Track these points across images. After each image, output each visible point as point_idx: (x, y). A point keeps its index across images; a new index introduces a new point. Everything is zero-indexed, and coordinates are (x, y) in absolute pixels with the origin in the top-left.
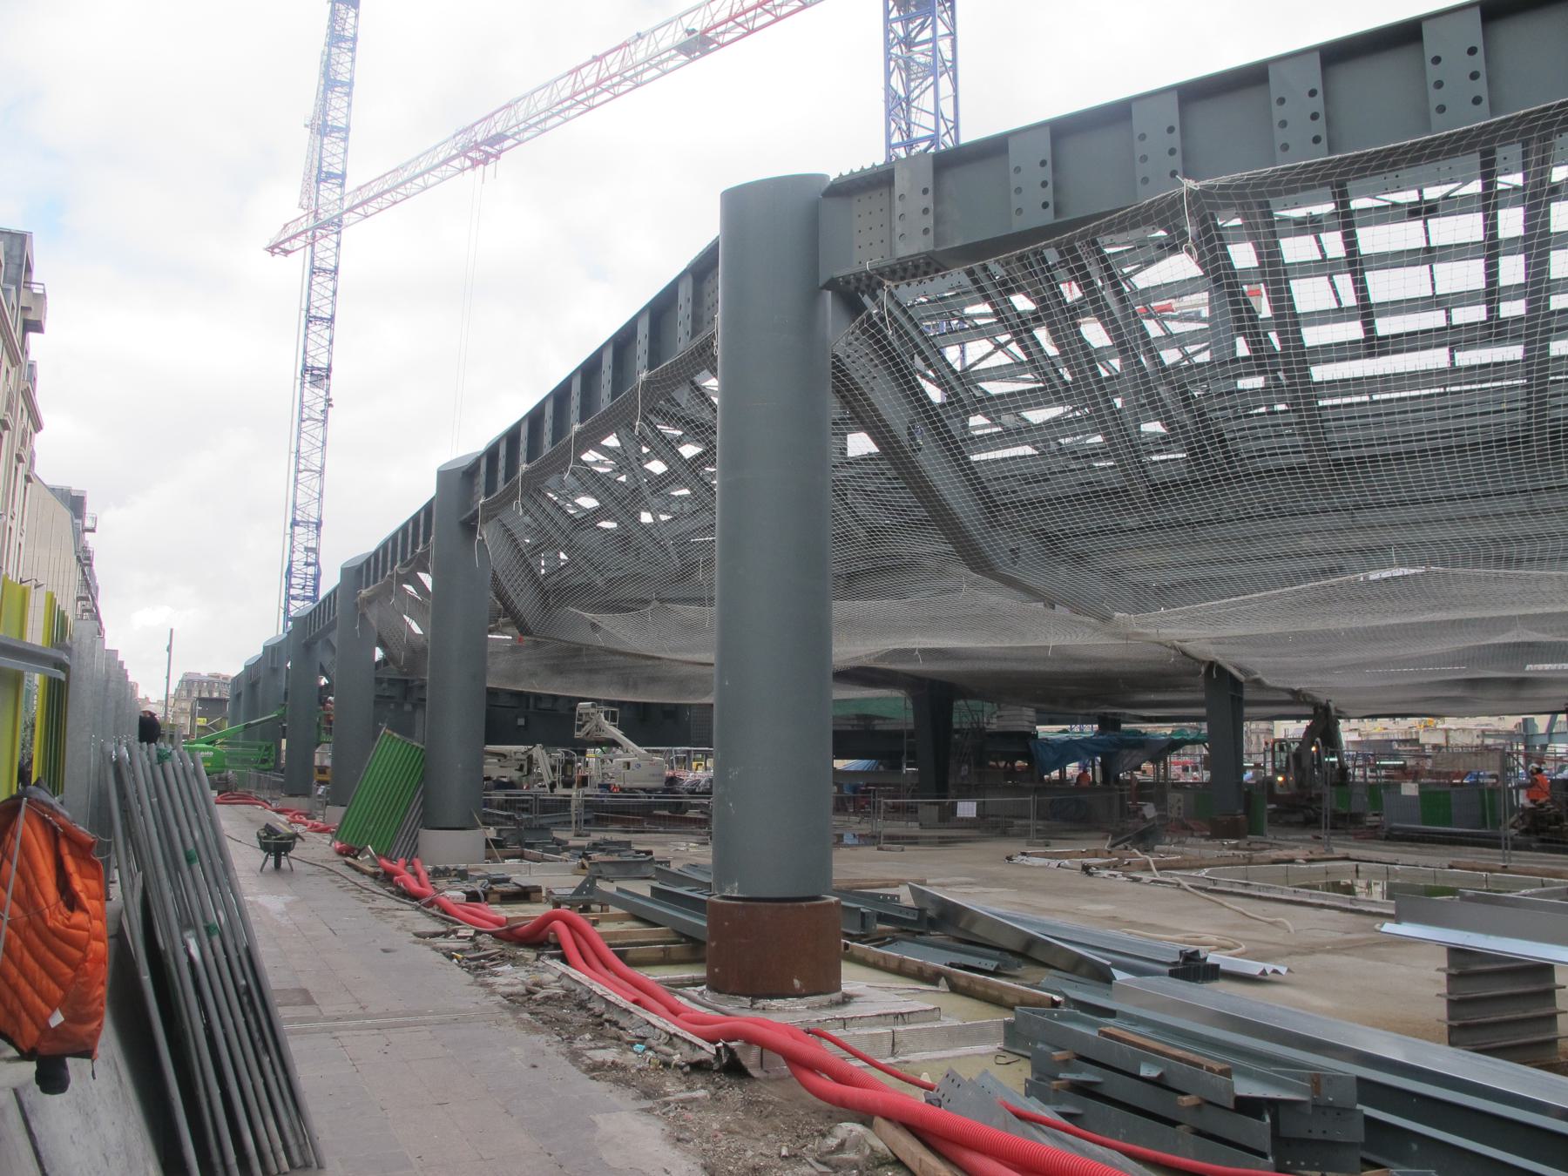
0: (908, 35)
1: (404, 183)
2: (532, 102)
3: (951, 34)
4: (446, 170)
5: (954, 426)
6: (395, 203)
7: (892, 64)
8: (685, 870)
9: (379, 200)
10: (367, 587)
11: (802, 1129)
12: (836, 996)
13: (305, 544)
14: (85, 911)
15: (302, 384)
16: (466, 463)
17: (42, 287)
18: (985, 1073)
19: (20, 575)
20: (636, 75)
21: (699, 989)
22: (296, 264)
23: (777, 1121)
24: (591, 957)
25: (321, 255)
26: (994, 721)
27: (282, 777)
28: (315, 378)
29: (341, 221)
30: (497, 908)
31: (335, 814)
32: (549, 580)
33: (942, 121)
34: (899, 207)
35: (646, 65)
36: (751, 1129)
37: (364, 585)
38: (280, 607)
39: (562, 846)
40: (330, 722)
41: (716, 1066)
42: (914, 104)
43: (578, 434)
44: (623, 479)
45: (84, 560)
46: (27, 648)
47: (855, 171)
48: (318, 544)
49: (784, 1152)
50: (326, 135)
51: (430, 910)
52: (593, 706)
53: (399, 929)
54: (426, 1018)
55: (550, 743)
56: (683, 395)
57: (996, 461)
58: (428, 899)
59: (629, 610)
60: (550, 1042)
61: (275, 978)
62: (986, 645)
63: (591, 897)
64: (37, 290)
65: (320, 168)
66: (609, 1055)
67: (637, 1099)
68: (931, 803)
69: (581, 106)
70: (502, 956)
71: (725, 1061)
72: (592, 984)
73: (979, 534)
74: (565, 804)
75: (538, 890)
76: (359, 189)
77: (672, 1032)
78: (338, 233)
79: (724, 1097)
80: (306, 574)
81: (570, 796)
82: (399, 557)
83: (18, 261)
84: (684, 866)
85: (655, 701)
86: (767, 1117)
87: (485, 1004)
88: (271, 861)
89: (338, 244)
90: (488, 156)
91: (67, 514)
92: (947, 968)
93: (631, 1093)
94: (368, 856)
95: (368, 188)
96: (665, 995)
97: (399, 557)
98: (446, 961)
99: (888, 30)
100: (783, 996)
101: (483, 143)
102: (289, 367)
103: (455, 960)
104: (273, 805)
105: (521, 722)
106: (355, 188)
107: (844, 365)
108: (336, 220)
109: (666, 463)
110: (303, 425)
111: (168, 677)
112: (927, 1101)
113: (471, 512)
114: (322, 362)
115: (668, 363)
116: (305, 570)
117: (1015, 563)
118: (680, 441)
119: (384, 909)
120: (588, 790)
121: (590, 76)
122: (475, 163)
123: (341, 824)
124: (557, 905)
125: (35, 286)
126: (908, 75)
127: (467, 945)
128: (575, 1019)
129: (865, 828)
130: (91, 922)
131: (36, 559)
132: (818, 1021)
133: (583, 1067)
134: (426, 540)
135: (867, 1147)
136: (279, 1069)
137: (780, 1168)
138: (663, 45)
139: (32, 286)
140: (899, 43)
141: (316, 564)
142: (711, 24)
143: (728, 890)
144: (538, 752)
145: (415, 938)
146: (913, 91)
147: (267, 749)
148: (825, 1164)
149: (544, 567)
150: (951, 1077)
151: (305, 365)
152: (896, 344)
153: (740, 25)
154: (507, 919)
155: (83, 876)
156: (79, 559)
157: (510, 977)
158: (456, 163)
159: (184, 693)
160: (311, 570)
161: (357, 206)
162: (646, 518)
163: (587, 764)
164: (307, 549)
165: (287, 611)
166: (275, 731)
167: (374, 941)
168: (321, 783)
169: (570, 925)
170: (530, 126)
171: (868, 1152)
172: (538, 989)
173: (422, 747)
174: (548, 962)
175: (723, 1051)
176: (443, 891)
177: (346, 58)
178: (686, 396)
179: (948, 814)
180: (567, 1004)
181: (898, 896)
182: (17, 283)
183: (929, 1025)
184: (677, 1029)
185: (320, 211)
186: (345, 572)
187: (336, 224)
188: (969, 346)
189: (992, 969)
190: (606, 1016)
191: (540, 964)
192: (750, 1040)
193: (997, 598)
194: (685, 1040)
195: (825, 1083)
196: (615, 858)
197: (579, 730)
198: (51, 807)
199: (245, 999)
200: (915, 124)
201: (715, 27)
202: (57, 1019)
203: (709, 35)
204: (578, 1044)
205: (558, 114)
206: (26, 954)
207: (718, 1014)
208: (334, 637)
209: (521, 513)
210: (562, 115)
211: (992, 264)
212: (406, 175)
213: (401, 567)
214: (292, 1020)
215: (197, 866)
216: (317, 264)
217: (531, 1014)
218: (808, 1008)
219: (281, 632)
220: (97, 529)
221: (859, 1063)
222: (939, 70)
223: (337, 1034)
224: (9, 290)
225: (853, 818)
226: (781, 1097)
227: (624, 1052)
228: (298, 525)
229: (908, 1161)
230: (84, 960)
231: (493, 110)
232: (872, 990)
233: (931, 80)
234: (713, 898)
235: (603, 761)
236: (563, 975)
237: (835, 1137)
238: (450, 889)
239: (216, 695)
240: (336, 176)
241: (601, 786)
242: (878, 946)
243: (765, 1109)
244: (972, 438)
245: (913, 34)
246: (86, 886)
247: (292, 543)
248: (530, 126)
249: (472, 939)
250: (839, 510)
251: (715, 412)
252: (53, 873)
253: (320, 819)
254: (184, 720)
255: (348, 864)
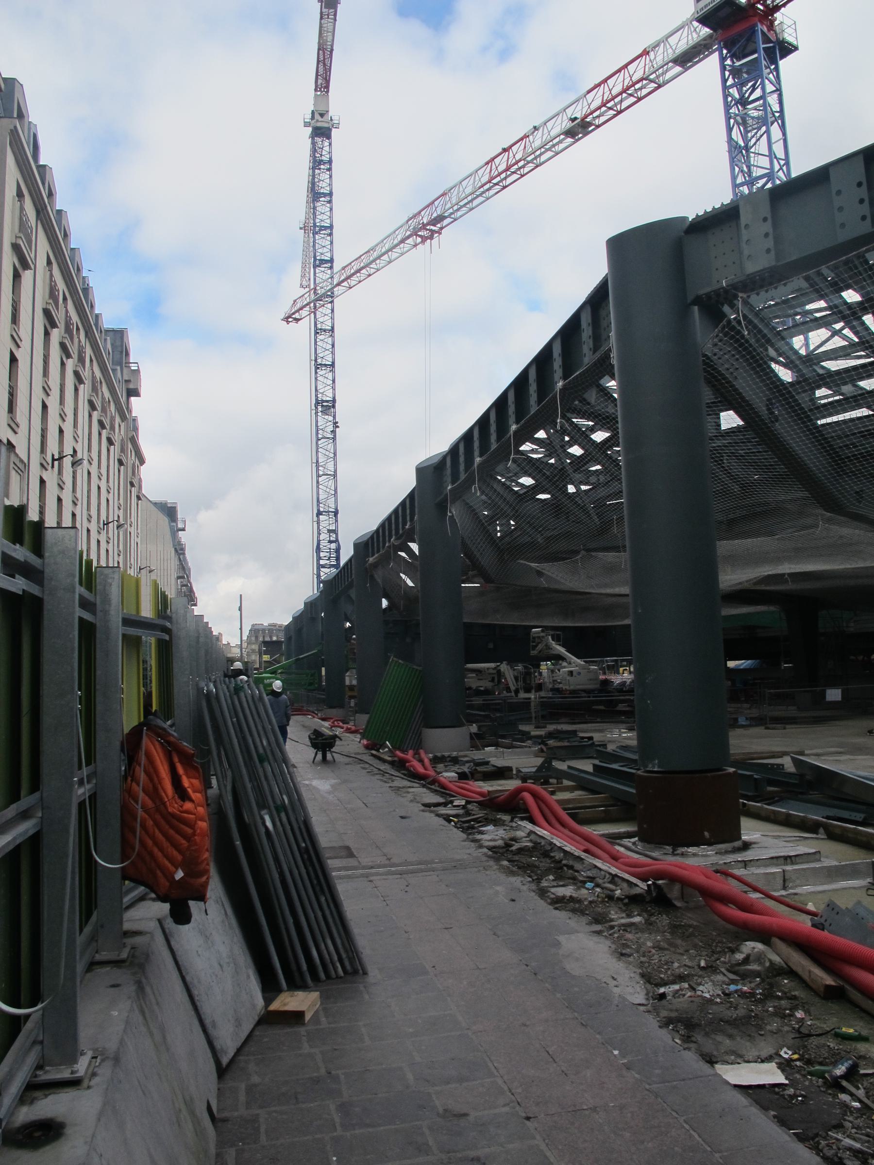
0: (742, 96)
1: (374, 261)
2: (461, 189)
3: (777, 90)
4: (405, 247)
5: (803, 399)
6: (370, 275)
7: (732, 121)
8: (618, 750)
9: (358, 274)
10: (373, 555)
11: (716, 946)
12: (737, 844)
13: (328, 527)
14: (192, 801)
15: (316, 413)
16: (436, 460)
17: (136, 365)
18: (859, 903)
19: (139, 565)
20: (535, 158)
21: (633, 840)
22: (305, 326)
23: (696, 941)
24: (552, 819)
25: (321, 320)
26: (852, 624)
27: (324, 695)
28: (325, 409)
29: (333, 293)
30: (480, 783)
31: (363, 719)
32: (503, 541)
33: (775, 160)
34: (745, 234)
35: (543, 150)
36: (676, 946)
37: (370, 555)
38: (313, 574)
39: (526, 736)
40: (354, 654)
41: (648, 899)
42: (752, 150)
43: (515, 432)
44: (552, 461)
45: (180, 550)
46: (142, 620)
47: (708, 211)
48: (337, 527)
49: (703, 964)
50: (317, 233)
51: (433, 787)
52: (542, 631)
53: (411, 801)
54: (434, 865)
55: (512, 662)
56: (592, 396)
57: (844, 422)
58: (431, 779)
59: (564, 559)
60: (524, 882)
61: (325, 839)
62: (842, 567)
63: (549, 773)
64: (134, 367)
65: (315, 257)
66: (567, 891)
67: (590, 924)
68: (805, 691)
69: (497, 187)
70: (486, 819)
71: (654, 894)
72: (552, 838)
73: (829, 482)
74: (527, 703)
75: (510, 769)
76: (344, 268)
77: (614, 873)
78: (332, 302)
79: (655, 922)
80: (330, 549)
81: (530, 698)
82: (393, 532)
83: (119, 349)
84: (617, 747)
85: (588, 625)
86: (688, 937)
87: (475, 855)
88: (320, 756)
89: (333, 311)
90: (433, 232)
91: (164, 520)
92: (824, 820)
93: (584, 920)
94: (387, 749)
95: (349, 267)
96: (608, 846)
97: (393, 532)
98: (446, 824)
99: (726, 96)
100: (697, 845)
101: (428, 224)
102: (305, 402)
103: (453, 823)
104: (319, 715)
105: (491, 646)
106: (340, 268)
107: (712, 361)
108: (329, 293)
109: (583, 448)
110: (320, 442)
111: (241, 629)
112: (813, 925)
113: (442, 496)
114: (328, 396)
115: (578, 373)
116: (329, 546)
117: (860, 502)
118: (593, 430)
119: (400, 787)
120: (543, 694)
121: (501, 163)
122: (424, 239)
123: (367, 727)
124: (524, 780)
125: (132, 365)
126: (745, 128)
127: (461, 812)
128: (541, 864)
129: (755, 713)
130: (196, 808)
131: (148, 552)
132: (725, 863)
133: (549, 901)
134: (412, 519)
135: (767, 961)
136: (332, 906)
137: (700, 976)
138: (554, 133)
139: (131, 365)
140: (736, 104)
141: (336, 541)
142: (589, 111)
143: (650, 766)
144: (504, 667)
145: (423, 808)
146: (750, 140)
147: (312, 675)
148: (734, 973)
149: (499, 531)
150: (831, 906)
151: (317, 399)
152: (752, 341)
153: (610, 108)
154: (488, 791)
155: (188, 777)
156: (176, 550)
157: (492, 834)
158: (410, 241)
159: (253, 639)
160: (333, 546)
161: (343, 281)
162: (571, 489)
163: (540, 674)
164: (330, 531)
165: (319, 576)
166: (315, 663)
167: (394, 810)
168: (351, 697)
169: (535, 795)
170: (462, 207)
171: (767, 964)
172: (514, 843)
173: (420, 668)
174: (520, 823)
175: (652, 887)
176: (441, 773)
177: (325, 176)
178: (594, 396)
179: (819, 699)
180: (535, 853)
181: (783, 765)
182: (120, 364)
183: (812, 865)
184: (617, 871)
185: (318, 288)
186: (356, 546)
187: (330, 296)
188: (811, 334)
189: (860, 820)
190: (564, 862)
191: (514, 825)
192: (673, 879)
193: (848, 531)
194: (623, 879)
195: (732, 911)
196: (566, 744)
197: (533, 650)
198: (164, 729)
199: (306, 856)
200: (754, 166)
201: (591, 113)
202: (179, 875)
203: (588, 120)
204: (544, 884)
205: (481, 195)
206: (157, 831)
207: (649, 859)
208: (353, 593)
209: (478, 494)
210: (484, 195)
211: (824, 270)
212: (375, 255)
213: (396, 539)
214: (339, 869)
215: (266, 764)
216: (319, 326)
217: (509, 861)
218: (716, 853)
219: (316, 592)
220: (186, 529)
221: (757, 895)
222: (770, 120)
223: (371, 878)
224: (116, 369)
225: (746, 705)
226: (699, 922)
227: (579, 888)
228: (322, 515)
229: (800, 971)
230: (194, 834)
231: (492, 156)
232: (764, 838)
233: (764, 129)
234: (639, 772)
235: (553, 671)
236: (531, 832)
237: (741, 952)
238: (446, 771)
239: (275, 639)
240: (326, 262)
241: (552, 690)
242: (768, 804)
243: (687, 930)
244: (818, 408)
245: (747, 95)
246: (191, 784)
247: (318, 528)
248: (462, 207)
249: (464, 807)
250: (717, 472)
251: (616, 405)
252: (169, 775)
253: (352, 723)
254: (255, 657)
255: (373, 755)
